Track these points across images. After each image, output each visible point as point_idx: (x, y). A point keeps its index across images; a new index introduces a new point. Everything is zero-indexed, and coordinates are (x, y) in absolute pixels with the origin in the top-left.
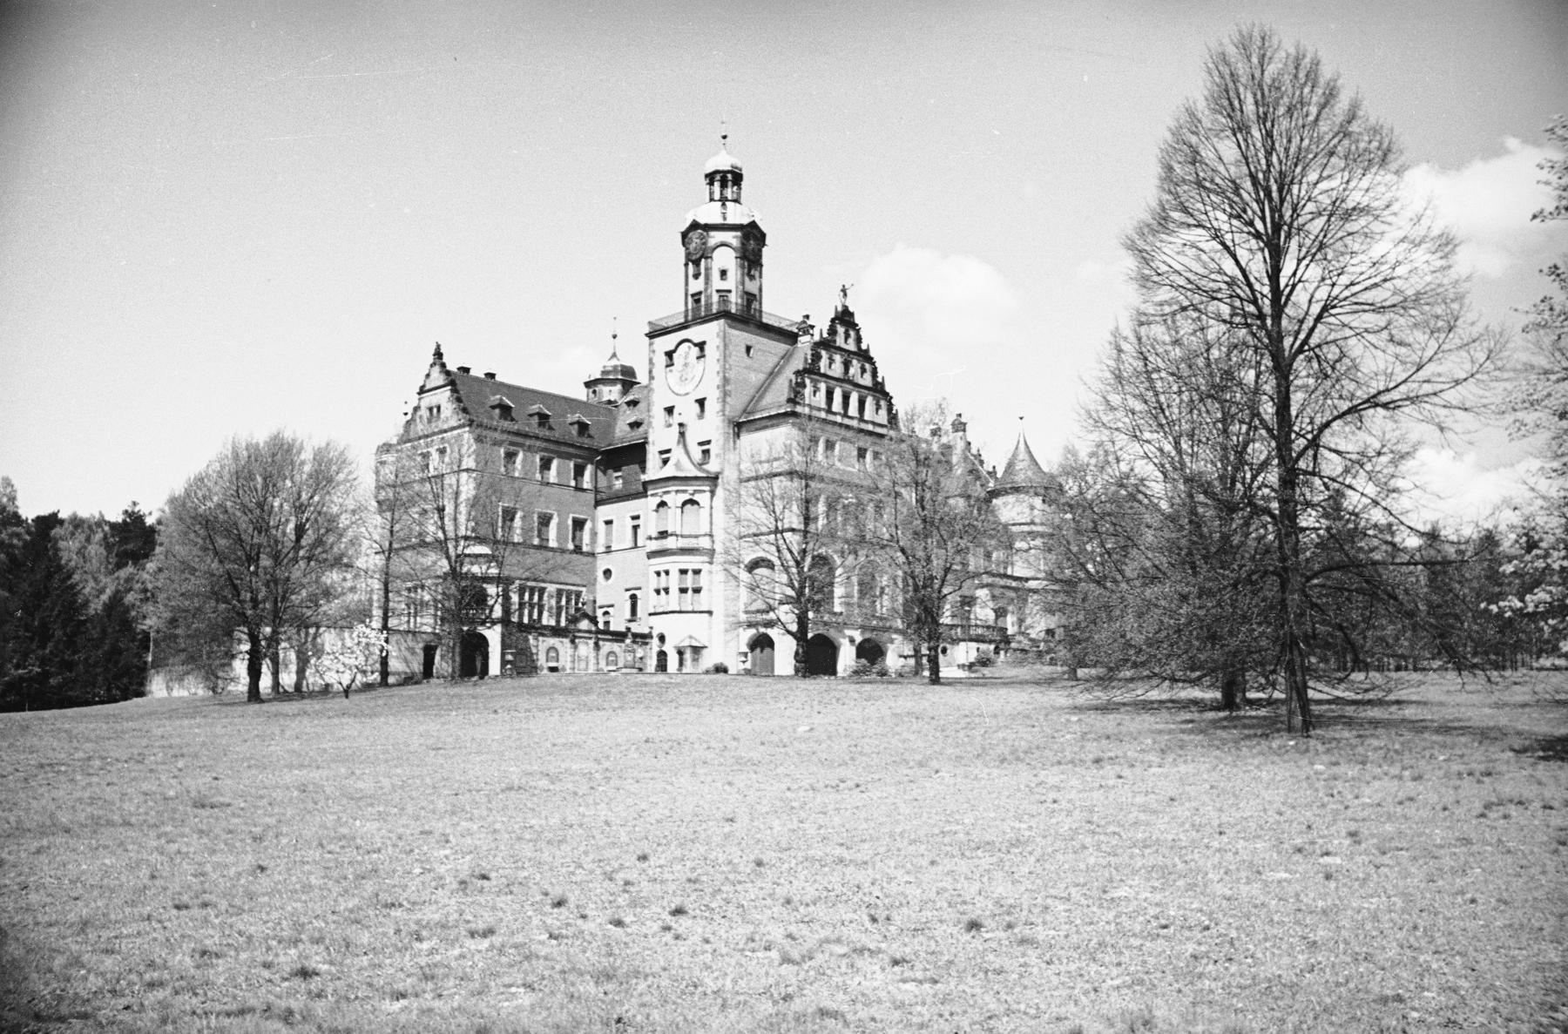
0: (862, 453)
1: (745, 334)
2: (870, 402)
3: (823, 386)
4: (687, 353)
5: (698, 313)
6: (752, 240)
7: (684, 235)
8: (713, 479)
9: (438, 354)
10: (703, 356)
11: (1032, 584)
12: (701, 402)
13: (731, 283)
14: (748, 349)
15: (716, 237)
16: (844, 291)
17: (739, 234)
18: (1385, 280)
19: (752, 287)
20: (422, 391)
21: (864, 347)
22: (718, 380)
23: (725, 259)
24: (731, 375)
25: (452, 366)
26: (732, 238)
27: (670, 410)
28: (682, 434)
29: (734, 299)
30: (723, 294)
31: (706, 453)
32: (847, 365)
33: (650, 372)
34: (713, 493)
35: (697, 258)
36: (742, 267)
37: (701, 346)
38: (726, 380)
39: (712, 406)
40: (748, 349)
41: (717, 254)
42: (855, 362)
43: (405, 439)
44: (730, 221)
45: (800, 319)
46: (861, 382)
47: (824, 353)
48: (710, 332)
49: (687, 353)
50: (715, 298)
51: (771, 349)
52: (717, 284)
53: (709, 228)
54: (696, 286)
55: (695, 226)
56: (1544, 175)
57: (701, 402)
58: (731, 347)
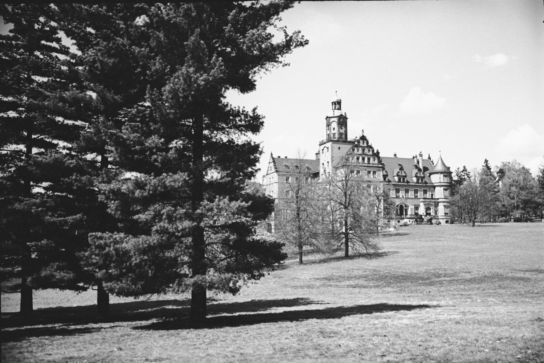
0: (369, 172)
1: (338, 145)
2: (372, 159)
4: (326, 149)
5: (329, 140)
6: (343, 121)
7: (326, 119)
9: (272, 154)
10: (317, 154)
11: (440, 200)
14: (339, 148)
15: (332, 120)
16: (363, 131)
20: (269, 163)
21: (369, 144)
22: (330, 157)
23: (334, 125)
24: (334, 155)
25: (275, 156)
26: (336, 119)
27: (323, 164)
28: (325, 170)
29: (337, 136)
30: (334, 134)
31: (329, 175)
32: (363, 150)
35: (328, 125)
36: (339, 127)
37: (328, 148)
38: (332, 157)
39: (330, 163)
40: (339, 148)
41: (332, 124)
42: (366, 149)
43: (267, 175)
44: (336, 115)
45: (355, 138)
46: (369, 154)
47: (355, 148)
48: (329, 145)
49: (326, 149)
50: (332, 136)
51: (346, 148)
52: (333, 132)
53: (330, 118)
54: (328, 132)
55: (327, 117)
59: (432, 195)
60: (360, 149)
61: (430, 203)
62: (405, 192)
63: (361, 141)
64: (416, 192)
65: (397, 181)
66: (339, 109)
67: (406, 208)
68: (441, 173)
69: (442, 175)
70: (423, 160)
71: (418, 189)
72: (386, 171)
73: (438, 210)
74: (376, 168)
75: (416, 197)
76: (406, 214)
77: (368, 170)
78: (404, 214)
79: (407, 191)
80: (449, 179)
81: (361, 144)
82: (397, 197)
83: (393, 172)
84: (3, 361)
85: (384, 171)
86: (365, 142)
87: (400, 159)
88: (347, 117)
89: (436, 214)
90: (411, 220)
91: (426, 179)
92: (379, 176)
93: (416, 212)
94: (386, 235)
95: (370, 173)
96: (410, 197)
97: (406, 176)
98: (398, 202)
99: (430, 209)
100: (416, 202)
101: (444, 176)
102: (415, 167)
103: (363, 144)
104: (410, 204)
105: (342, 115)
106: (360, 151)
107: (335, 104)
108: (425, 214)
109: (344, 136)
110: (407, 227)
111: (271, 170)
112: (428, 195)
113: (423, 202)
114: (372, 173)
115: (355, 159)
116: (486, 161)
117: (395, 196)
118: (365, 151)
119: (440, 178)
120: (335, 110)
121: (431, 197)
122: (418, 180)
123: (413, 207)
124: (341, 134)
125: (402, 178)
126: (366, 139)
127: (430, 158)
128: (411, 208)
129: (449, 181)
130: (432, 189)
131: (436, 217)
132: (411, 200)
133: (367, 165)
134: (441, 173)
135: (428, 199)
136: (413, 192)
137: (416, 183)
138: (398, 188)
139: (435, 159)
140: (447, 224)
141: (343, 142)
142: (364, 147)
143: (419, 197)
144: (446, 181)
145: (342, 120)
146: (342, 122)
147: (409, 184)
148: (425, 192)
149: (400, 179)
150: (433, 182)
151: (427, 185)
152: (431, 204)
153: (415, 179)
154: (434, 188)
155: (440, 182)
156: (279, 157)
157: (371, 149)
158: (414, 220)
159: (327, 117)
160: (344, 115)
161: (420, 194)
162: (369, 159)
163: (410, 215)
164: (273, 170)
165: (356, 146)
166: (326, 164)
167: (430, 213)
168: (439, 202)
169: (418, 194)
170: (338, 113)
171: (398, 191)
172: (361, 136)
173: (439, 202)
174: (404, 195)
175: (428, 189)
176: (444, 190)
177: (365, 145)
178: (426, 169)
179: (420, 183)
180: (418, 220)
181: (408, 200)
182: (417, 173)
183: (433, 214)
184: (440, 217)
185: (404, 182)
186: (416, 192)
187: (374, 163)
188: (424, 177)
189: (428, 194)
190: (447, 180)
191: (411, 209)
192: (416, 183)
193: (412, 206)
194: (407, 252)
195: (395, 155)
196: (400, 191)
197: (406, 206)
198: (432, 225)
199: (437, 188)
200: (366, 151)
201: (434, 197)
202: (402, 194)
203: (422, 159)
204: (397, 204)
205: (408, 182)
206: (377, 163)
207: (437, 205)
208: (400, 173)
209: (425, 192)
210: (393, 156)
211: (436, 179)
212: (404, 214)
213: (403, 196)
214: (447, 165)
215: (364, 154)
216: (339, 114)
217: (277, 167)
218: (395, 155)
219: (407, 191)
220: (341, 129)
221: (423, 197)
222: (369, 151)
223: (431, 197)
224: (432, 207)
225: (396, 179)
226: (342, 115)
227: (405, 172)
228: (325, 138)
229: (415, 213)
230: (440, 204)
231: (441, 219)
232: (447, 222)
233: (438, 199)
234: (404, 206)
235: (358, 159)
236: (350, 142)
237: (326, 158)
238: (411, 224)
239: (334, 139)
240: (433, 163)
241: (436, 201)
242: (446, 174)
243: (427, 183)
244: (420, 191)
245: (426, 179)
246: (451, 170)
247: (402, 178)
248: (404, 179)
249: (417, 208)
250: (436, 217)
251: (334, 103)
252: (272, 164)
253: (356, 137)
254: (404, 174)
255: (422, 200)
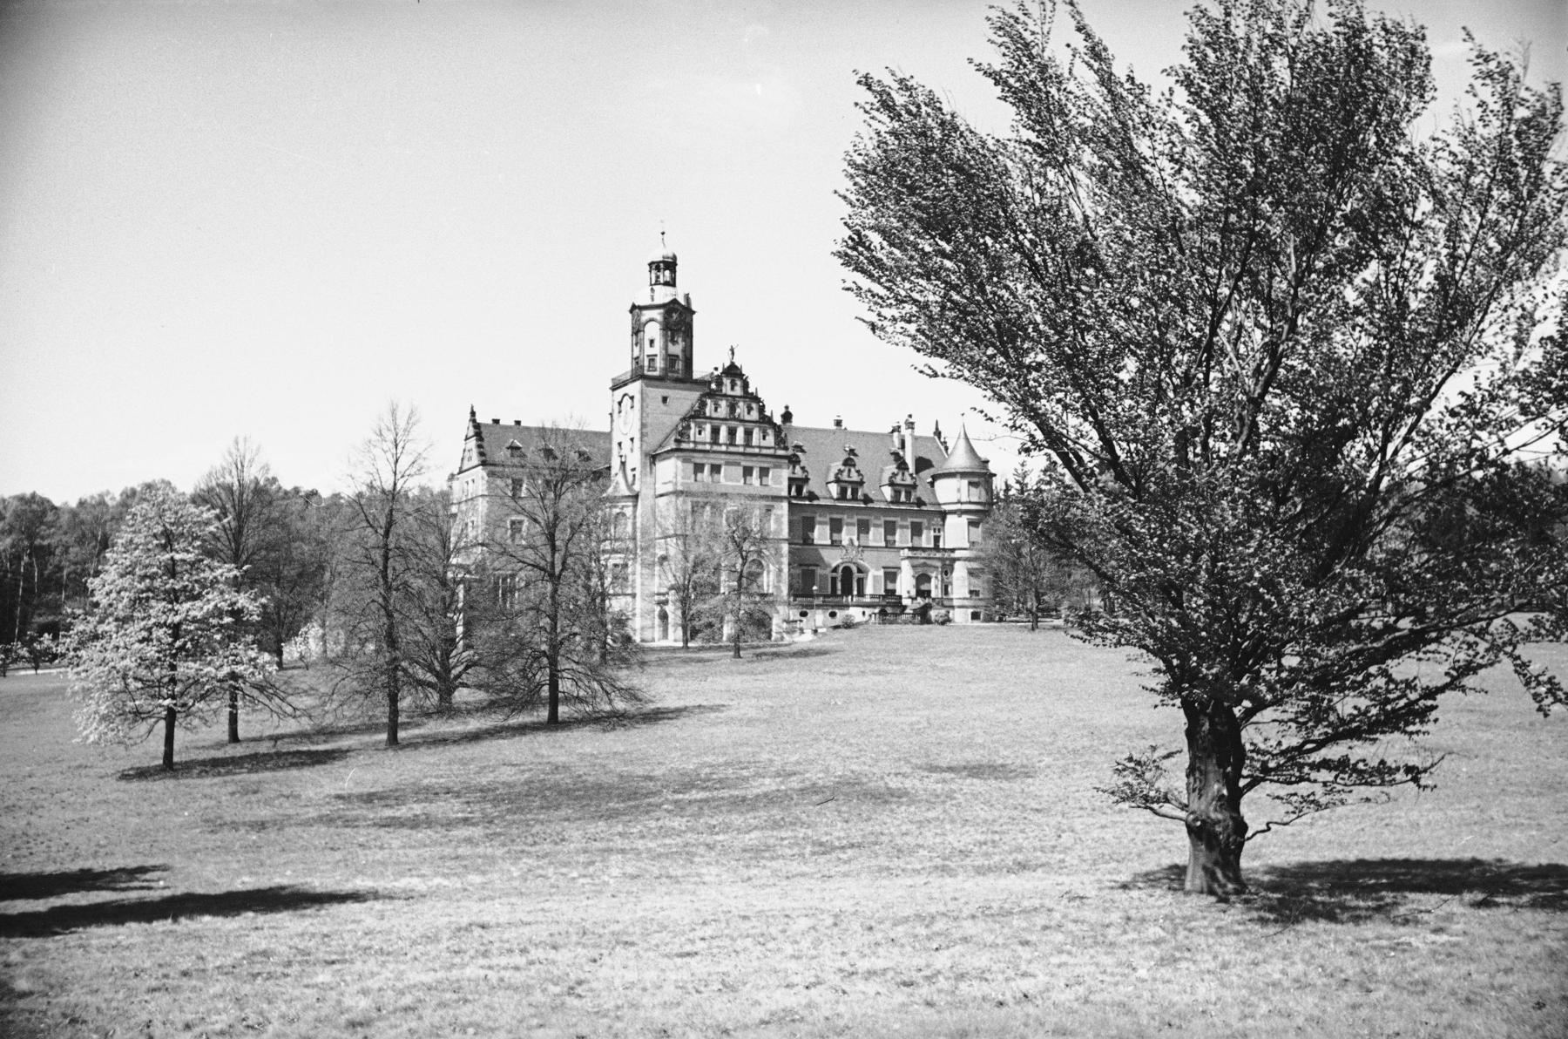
0: (748, 471)
2: (756, 434)
3: (708, 427)
4: (627, 400)
5: (638, 375)
6: (678, 320)
7: (631, 311)
8: (636, 497)
9: (473, 414)
11: (957, 554)
12: (632, 440)
13: (657, 349)
14: (665, 399)
15: (647, 315)
17: (662, 311)
18: (79, 767)
19: (676, 349)
21: (751, 390)
22: (637, 425)
23: (653, 331)
24: (649, 420)
26: (657, 314)
27: (620, 444)
29: (659, 363)
30: (652, 359)
32: (733, 408)
33: (612, 421)
34: (635, 506)
35: (637, 330)
36: (665, 336)
37: (632, 398)
38: (643, 425)
39: (637, 442)
40: (665, 399)
41: (647, 328)
42: (741, 404)
43: (461, 472)
46: (747, 418)
47: (709, 401)
48: (635, 388)
49: (627, 400)
50: (1364, 285)
51: (685, 399)
52: (648, 351)
53: (642, 308)
54: (636, 353)
55: (634, 307)
56: (924, 429)
57: (632, 440)
58: (648, 401)
59: (937, 539)
60: (723, 403)
61: (929, 562)
62: (859, 532)
63: (727, 381)
64: (890, 529)
65: (835, 496)
66: (672, 283)
67: (861, 575)
68: (963, 475)
69: (965, 482)
70: (916, 439)
71: (898, 519)
72: (803, 468)
73: (951, 583)
74: (769, 459)
75: (890, 545)
76: (861, 593)
77: (743, 463)
78: (855, 593)
79: (864, 528)
80: (983, 492)
81: (727, 389)
82: (835, 544)
83: (828, 469)
84: (3, 939)
85: (798, 468)
86: (739, 383)
87: (852, 433)
88: (694, 308)
89: (946, 592)
90: (868, 611)
91: (921, 492)
92: (777, 480)
93: (890, 586)
94: (765, 654)
95: (751, 475)
96: (871, 544)
97: (861, 483)
98: (834, 558)
99: (928, 579)
100: (889, 558)
101: (970, 484)
102: (892, 458)
103: (732, 389)
104: (871, 563)
105: (675, 301)
106: (723, 410)
107: (658, 269)
108: (913, 593)
109: (680, 365)
110: (847, 632)
111: (470, 459)
112: (926, 540)
113: (908, 558)
114: (756, 473)
115: (707, 435)
116: (787, 407)
117: (829, 542)
118: (738, 411)
119: (959, 490)
120: (655, 287)
121: (932, 546)
122: (897, 493)
123: (881, 573)
124: (671, 359)
125: (851, 489)
126: (741, 375)
127: (938, 433)
128: (875, 577)
129: (983, 500)
130: (938, 520)
131: (945, 602)
132: (875, 553)
133: (741, 450)
134: (963, 475)
135: (924, 550)
136: (882, 530)
137: (892, 502)
138: (838, 516)
139: (951, 435)
140: (976, 623)
141: (677, 380)
142: (734, 397)
143: (898, 544)
144: (975, 499)
145: (675, 316)
146: (677, 323)
147: (870, 505)
148: (917, 530)
149: (843, 491)
150: (941, 501)
151: (924, 508)
152: (931, 566)
153: (888, 492)
154: (944, 520)
155: (959, 502)
156: (496, 421)
157: (754, 405)
158: (877, 610)
159: (634, 307)
160: (682, 302)
161: (902, 537)
162: (748, 433)
163: (872, 596)
164: (476, 460)
165: (712, 394)
166: (626, 444)
167: (929, 592)
168: (954, 560)
169: (897, 537)
170: (663, 295)
171: (836, 527)
172: (727, 364)
173: (954, 560)
174: (855, 538)
175: (925, 521)
176: (972, 523)
177: (738, 391)
178: (922, 464)
179: (903, 503)
180: (889, 610)
181: (867, 553)
182: (894, 475)
183: (936, 593)
184: (956, 603)
185: (854, 499)
186: (890, 529)
187: (764, 443)
188: (914, 486)
189: (924, 536)
190: (977, 495)
191: (875, 577)
192: (892, 502)
193: (877, 569)
194: (748, 708)
195: (838, 423)
196: (845, 528)
197: (860, 571)
198: (926, 627)
199: (950, 519)
200: (741, 408)
201: (941, 546)
202: (848, 535)
203: (912, 435)
204: (834, 565)
205: (867, 500)
206: (708, 440)
207: (947, 568)
208: (845, 474)
209: (917, 530)
210: (832, 427)
211: (949, 492)
212: (855, 593)
213: (851, 540)
214: (982, 455)
215: (735, 419)
216: (667, 300)
217: (487, 449)
218: (838, 423)
219: (864, 528)
220: (674, 342)
221: (910, 545)
222: (750, 409)
223: (932, 546)
224: (933, 575)
225: (834, 489)
226: (675, 301)
227: (858, 472)
228: (625, 368)
229: (886, 590)
230: (957, 565)
231: (960, 607)
232: (975, 616)
233: (953, 550)
234: (854, 569)
235: (715, 431)
236: (702, 383)
237: (627, 428)
238: (867, 622)
239: (650, 373)
240: (946, 449)
241: (946, 555)
242: (976, 480)
243: (925, 504)
244: (848, 524)
245: (921, 492)
246: (992, 468)
247: (851, 489)
248: (855, 492)
249: (891, 575)
250: (946, 603)
251: (655, 266)
252: (473, 443)
253: (716, 369)
254: (855, 477)
255: (907, 553)
